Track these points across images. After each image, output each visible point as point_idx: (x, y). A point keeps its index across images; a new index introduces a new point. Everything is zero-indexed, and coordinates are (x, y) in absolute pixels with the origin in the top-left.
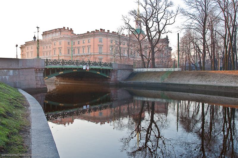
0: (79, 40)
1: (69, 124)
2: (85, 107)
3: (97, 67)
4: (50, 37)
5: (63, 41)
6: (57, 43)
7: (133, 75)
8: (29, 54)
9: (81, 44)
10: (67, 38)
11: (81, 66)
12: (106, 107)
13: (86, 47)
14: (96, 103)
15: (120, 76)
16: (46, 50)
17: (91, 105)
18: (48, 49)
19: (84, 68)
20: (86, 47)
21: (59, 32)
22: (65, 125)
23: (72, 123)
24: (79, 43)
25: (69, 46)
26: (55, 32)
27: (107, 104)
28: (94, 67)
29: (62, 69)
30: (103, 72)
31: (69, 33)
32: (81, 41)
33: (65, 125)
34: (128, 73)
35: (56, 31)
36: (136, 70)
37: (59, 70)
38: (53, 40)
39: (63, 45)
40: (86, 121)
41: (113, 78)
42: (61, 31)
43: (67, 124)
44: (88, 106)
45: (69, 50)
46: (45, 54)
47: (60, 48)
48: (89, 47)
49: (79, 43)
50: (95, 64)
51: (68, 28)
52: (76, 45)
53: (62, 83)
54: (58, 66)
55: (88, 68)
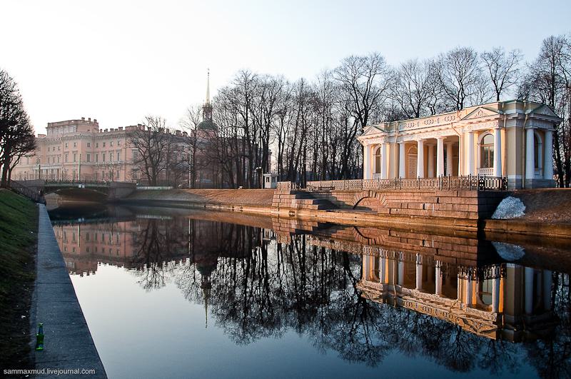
0: (104, 141)
1: (88, 275)
2: (80, 220)
3: (93, 185)
4: (59, 133)
5: (79, 142)
6: (71, 143)
7: (135, 192)
8: (72, 239)
9: (108, 148)
10: (86, 138)
11: (77, 185)
12: (102, 222)
13: (115, 152)
14: (92, 218)
15: (119, 194)
16: (54, 153)
17: (86, 218)
18: (57, 152)
19: (80, 186)
20: (115, 152)
21: (75, 126)
22: (82, 276)
23: (94, 273)
24: (104, 146)
25: (89, 150)
26: (69, 125)
27: (104, 219)
28: (89, 185)
29: (59, 187)
30: (101, 190)
31: (91, 128)
32: (108, 143)
33: (82, 276)
34: (129, 191)
35: (69, 123)
36: (138, 188)
37: (56, 188)
38: (63, 139)
39: (79, 149)
40: (114, 268)
41: (111, 195)
42: (77, 125)
43: (85, 274)
44: (83, 219)
45: (88, 155)
46: (51, 159)
47: (75, 153)
48: (119, 152)
49: (104, 146)
50: (91, 183)
51: (90, 119)
52: (101, 148)
53: (65, 201)
54: (55, 185)
55: (83, 187)
